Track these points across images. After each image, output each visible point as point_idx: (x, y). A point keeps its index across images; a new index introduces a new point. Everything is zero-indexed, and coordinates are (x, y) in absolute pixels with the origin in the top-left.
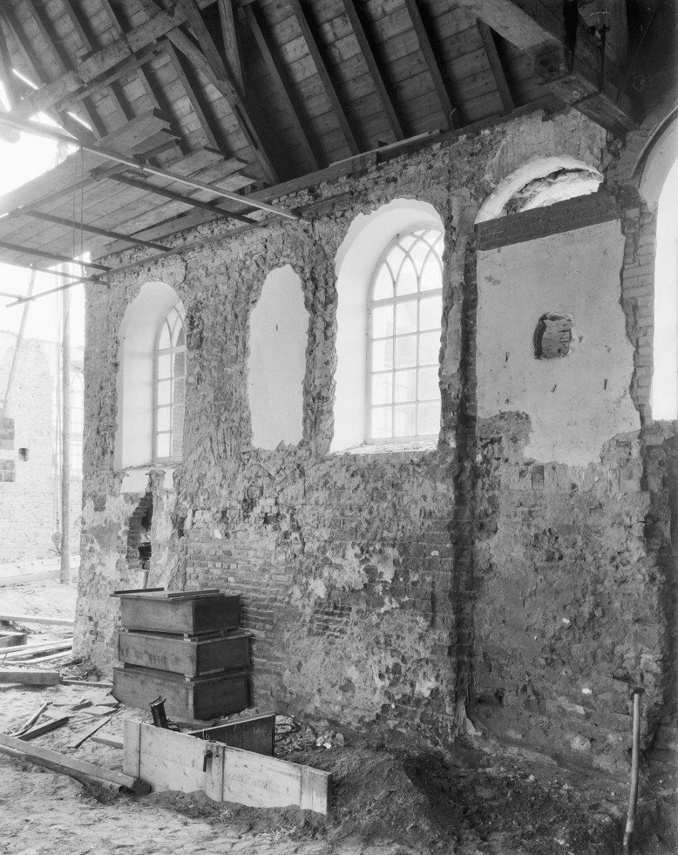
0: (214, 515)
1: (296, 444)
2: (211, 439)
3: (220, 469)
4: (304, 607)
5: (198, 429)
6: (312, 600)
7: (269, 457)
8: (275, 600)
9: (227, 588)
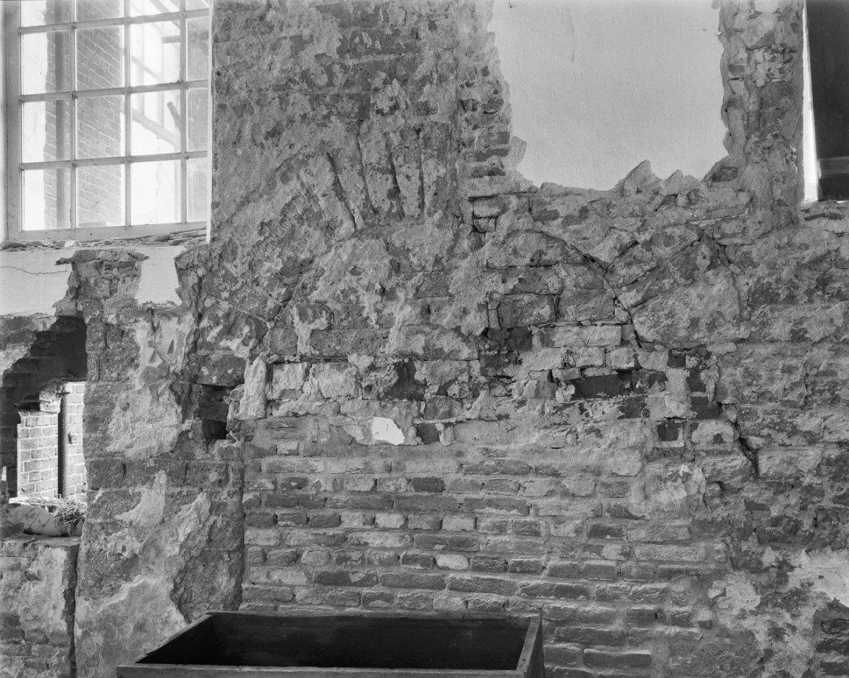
0: (359, 378)
1: (699, 172)
2: (331, 160)
3: (378, 244)
4: (777, 633)
5: (274, 133)
6: (807, 614)
7: (584, 212)
8: (657, 617)
9: (439, 585)
